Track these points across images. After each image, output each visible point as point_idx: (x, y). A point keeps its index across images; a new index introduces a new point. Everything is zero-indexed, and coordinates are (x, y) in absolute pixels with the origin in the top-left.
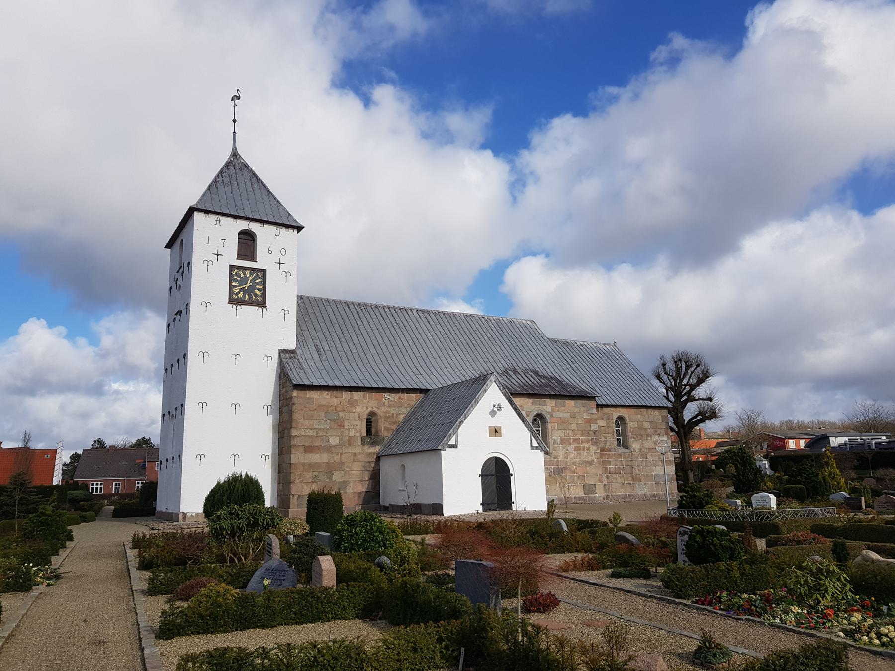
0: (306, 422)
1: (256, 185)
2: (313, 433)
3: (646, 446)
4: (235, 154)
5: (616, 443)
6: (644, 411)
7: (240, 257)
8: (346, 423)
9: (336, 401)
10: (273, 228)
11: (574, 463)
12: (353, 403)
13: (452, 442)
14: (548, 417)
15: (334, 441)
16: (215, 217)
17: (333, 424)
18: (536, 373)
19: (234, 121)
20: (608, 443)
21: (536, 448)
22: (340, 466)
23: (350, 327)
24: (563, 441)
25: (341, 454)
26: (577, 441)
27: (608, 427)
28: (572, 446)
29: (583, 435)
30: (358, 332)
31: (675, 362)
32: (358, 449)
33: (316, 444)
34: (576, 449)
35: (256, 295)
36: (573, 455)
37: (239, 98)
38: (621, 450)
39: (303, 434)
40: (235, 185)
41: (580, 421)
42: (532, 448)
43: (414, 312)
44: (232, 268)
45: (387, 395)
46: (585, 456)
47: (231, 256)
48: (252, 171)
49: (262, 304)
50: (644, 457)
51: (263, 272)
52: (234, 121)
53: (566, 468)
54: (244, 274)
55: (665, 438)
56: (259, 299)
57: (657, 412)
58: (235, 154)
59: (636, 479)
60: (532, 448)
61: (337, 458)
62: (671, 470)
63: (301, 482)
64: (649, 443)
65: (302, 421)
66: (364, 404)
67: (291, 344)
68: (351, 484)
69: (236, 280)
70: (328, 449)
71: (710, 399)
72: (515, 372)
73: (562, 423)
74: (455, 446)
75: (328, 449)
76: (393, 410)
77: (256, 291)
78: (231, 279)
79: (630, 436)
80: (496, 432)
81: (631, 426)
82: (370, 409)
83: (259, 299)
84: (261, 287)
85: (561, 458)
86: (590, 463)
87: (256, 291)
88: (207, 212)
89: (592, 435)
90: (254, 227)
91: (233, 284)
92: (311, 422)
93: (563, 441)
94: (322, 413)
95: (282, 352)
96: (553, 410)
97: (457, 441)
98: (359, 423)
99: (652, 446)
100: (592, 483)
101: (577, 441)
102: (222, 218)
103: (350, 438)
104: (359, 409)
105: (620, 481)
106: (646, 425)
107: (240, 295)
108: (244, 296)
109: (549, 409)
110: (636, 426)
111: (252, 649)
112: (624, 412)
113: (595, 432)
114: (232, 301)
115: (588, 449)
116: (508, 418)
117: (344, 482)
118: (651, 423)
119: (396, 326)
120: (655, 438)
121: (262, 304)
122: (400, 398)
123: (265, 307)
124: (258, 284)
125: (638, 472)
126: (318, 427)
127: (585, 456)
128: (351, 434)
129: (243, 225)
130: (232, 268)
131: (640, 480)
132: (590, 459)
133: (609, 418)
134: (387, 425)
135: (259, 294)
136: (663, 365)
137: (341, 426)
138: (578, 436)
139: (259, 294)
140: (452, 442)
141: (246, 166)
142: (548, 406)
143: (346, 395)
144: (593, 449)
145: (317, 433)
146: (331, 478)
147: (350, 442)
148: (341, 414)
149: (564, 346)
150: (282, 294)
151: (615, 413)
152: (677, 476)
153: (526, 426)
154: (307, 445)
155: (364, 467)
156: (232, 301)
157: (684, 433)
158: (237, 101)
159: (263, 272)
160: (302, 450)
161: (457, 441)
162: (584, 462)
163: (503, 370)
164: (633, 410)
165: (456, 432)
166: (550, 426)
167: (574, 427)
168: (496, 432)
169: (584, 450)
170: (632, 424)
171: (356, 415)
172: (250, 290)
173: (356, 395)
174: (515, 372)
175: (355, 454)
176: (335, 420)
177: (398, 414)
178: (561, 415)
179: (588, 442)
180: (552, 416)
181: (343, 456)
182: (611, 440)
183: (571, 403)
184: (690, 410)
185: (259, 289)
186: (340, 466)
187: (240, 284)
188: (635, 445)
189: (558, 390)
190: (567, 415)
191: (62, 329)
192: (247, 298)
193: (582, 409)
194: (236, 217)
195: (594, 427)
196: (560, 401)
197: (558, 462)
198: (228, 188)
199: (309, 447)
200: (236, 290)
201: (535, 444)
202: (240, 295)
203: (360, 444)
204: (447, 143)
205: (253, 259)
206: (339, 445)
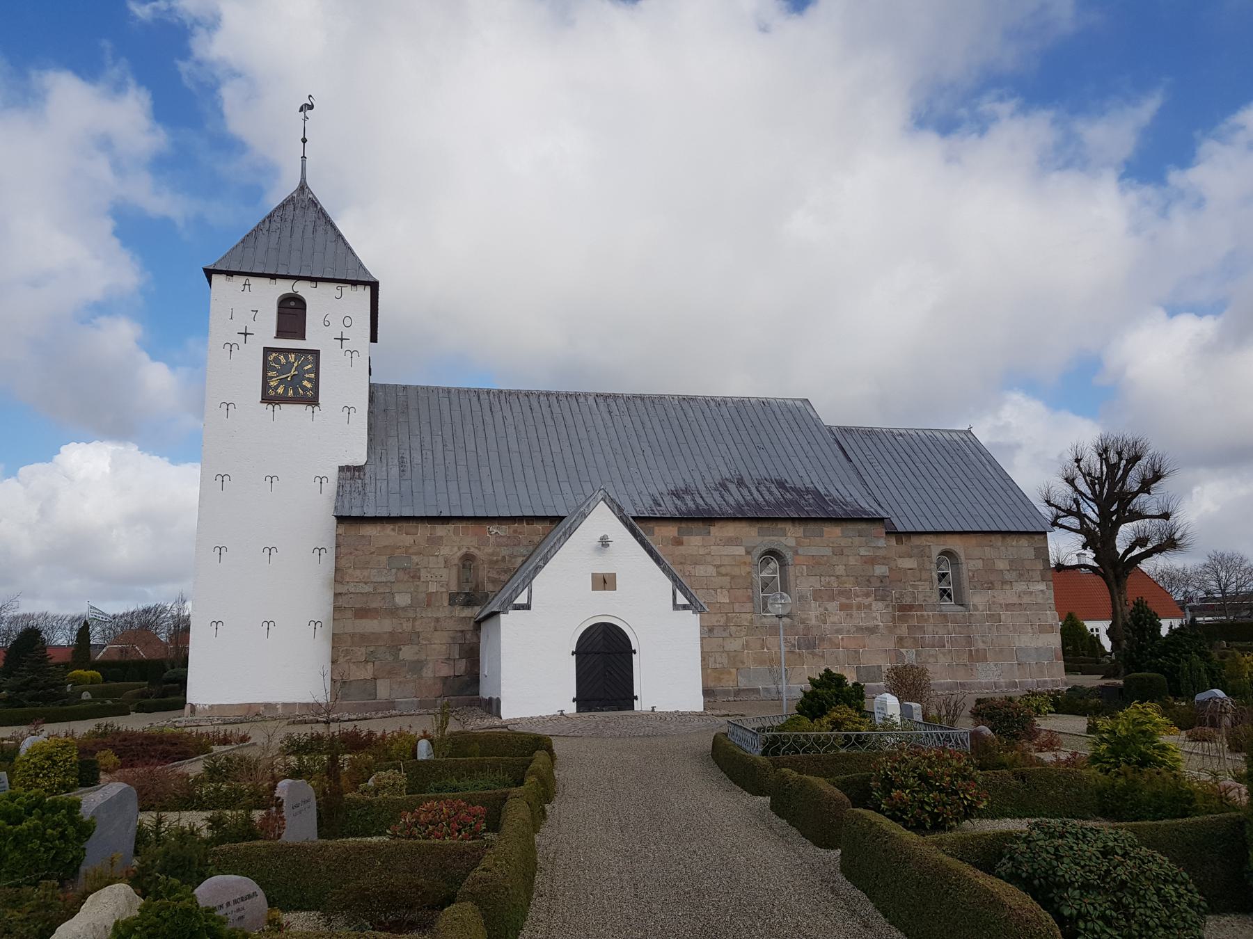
0: (358, 572)
1: (320, 230)
2: (367, 589)
4: (303, 187)
5: (936, 595)
6: (997, 540)
7: (281, 334)
8: (423, 573)
9: (408, 540)
10: (332, 287)
11: (838, 631)
12: (434, 542)
13: (522, 599)
14: (789, 555)
15: (402, 600)
16: (243, 279)
17: (401, 575)
18: (781, 485)
19: (304, 141)
20: (921, 597)
21: (685, 607)
22: (414, 638)
23: (469, 428)
24: (817, 595)
25: (415, 619)
26: (846, 593)
28: (836, 603)
29: (858, 584)
30: (480, 433)
31: (1100, 455)
32: (443, 611)
33: (374, 605)
34: (843, 607)
35: (304, 388)
36: (836, 617)
37: (311, 107)
38: (949, 607)
39: (352, 590)
40: (287, 232)
41: (852, 561)
42: (676, 606)
43: (591, 400)
44: (267, 351)
45: (494, 529)
46: (860, 618)
47: (266, 332)
48: (322, 209)
49: (313, 401)
50: (995, 619)
51: (316, 353)
52: (304, 141)
53: (822, 639)
54: (287, 358)
55: (1042, 586)
56: (310, 394)
57: (1024, 542)
58: (303, 187)
59: (977, 657)
60: (676, 606)
61: (407, 626)
62: (1055, 640)
63: (348, 661)
64: (1007, 595)
65: (350, 571)
66: (454, 542)
67: (359, 456)
68: (431, 665)
69: (273, 369)
70: (393, 612)
71: (1166, 516)
72: (741, 483)
73: (817, 565)
74: (527, 607)
75: (393, 612)
76: (504, 551)
77: (305, 383)
78: (266, 366)
79: (966, 583)
80: (604, 582)
81: (970, 566)
82: (464, 550)
83: (272, 393)
84: (270, 374)
85: (813, 622)
86: (872, 630)
87: (305, 383)
88: (230, 273)
90: (303, 289)
91: (270, 374)
92: (366, 573)
93: (817, 595)
94: (384, 559)
95: (341, 469)
96: (798, 544)
97: (529, 598)
98: (445, 572)
99: (1015, 600)
100: (874, 663)
101: (846, 593)
102: (252, 280)
103: (430, 595)
104: (445, 551)
105: (943, 660)
106: (1001, 565)
107: (280, 390)
108: (286, 390)
109: (791, 542)
110: (981, 566)
111: (469, 904)
112: (954, 544)
113: (882, 579)
114: (267, 398)
115: (869, 607)
116: (629, 557)
117: (419, 661)
118: (1011, 562)
119: (549, 422)
120: (1020, 587)
121: (313, 401)
122: (515, 531)
123: (317, 404)
124: (308, 371)
125: (981, 646)
127: (860, 618)
128: (432, 588)
129: (285, 287)
130: (267, 351)
131: (985, 659)
132: (871, 624)
133: (923, 554)
134: (494, 575)
135: (309, 386)
136: (1078, 461)
137: (416, 577)
138: (848, 586)
139: (309, 386)
140: (522, 599)
141: (314, 203)
142: (789, 538)
143: (424, 531)
144: (879, 607)
145: (375, 588)
146: (396, 656)
147: (430, 601)
148: (415, 559)
149: (847, 442)
150: (344, 385)
151: (936, 547)
152: (1065, 652)
153: (664, 570)
155: (453, 638)
156: (267, 398)
157: (1117, 577)
158: (308, 113)
159: (316, 353)
160: (350, 614)
161: (529, 598)
162: (859, 629)
163: (718, 479)
164: (973, 540)
165: (527, 582)
166: (791, 569)
167: (840, 570)
168: (604, 582)
169: (859, 608)
170: (971, 563)
171: (441, 560)
172: (296, 381)
173: (440, 530)
174: (741, 483)
175: (437, 620)
176: (405, 569)
177: (512, 556)
178: (814, 551)
179: (867, 595)
180: (796, 553)
181: (418, 623)
182: (927, 591)
183: (834, 532)
184: (1126, 533)
185: (309, 380)
186: (414, 638)
187: (280, 372)
188: (977, 599)
189: (811, 511)
190: (827, 551)
191: (166, 459)
192: (291, 393)
193: (857, 540)
194: (273, 277)
195: (880, 570)
196: (812, 527)
197: (807, 628)
198: (274, 237)
199: (361, 609)
201: (682, 600)
202: (280, 390)
203: (446, 604)
204: (1068, 165)
206: (410, 606)
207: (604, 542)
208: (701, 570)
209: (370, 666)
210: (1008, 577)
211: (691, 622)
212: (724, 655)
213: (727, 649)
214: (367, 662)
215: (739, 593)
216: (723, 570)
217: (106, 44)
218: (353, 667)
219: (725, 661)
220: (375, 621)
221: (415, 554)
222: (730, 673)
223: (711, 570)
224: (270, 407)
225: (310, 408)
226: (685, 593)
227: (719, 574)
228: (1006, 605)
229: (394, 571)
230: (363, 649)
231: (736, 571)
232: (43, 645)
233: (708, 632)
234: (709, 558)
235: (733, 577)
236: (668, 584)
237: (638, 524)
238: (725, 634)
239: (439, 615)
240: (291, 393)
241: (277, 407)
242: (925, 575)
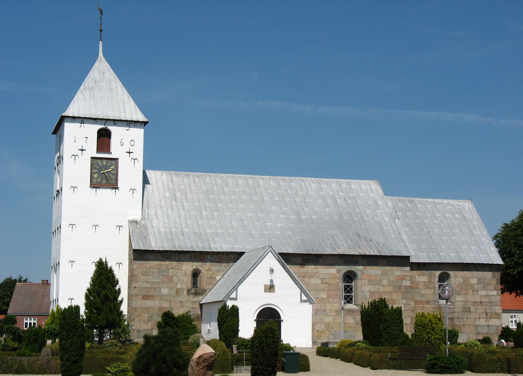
0: (144, 277)
2: (148, 285)
3: (471, 298)
15: (165, 291)
17: (164, 279)
19: (101, 31)
21: (305, 301)
25: (170, 301)
27: (430, 281)
33: (151, 294)
39: (141, 286)
41: (392, 278)
42: (302, 301)
47: (92, 151)
49: (115, 187)
52: (101, 31)
54: (102, 163)
60: (302, 301)
89: (403, 290)
92: (147, 277)
94: (156, 271)
97: (236, 295)
98: (185, 279)
103: (177, 290)
107: (99, 180)
108: (102, 181)
113: (406, 288)
116: (282, 277)
123: (118, 188)
126: (153, 281)
128: (179, 286)
147: (178, 292)
154: (144, 294)
159: (116, 159)
160: (140, 297)
161: (236, 295)
167: (385, 282)
171: (183, 272)
175: (181, 302)
180: (363, 273)
181: (172, 303)
185: (113, 174)
200: (96, 176)
201: (304, 298)
205: (108, 151)
207: (272, 271)
208: (313, 281)
209: (150, 323)
210: (476, 287)
211: (308, 308)
212: (323, 324)
213: (325, 321)
214: (148, 321)
215: (332, 293)
216: (325, 281)
217: (103, 92)
218: (142, 323)
219: (323, 327)
220: (152, 302)
221: (171, 269)
222: (325, 333)
223: (318, 281)
224: (95, 189)
225: (114, 190)
226: (306, 295)
227: (322, 283)
228: (474, 302)
229: (160, 277)
230: (146, 315)
231: (331, 281)
232: (386, 306)
233: (316, 312)
234: (317, 275)
235: (330, 285)
236: (299, 291)
237: (287, 259)
238: (324, 314)
239: (182, 299)
240: (104, 182)
241: (98, 190)
242: (431, 285)
